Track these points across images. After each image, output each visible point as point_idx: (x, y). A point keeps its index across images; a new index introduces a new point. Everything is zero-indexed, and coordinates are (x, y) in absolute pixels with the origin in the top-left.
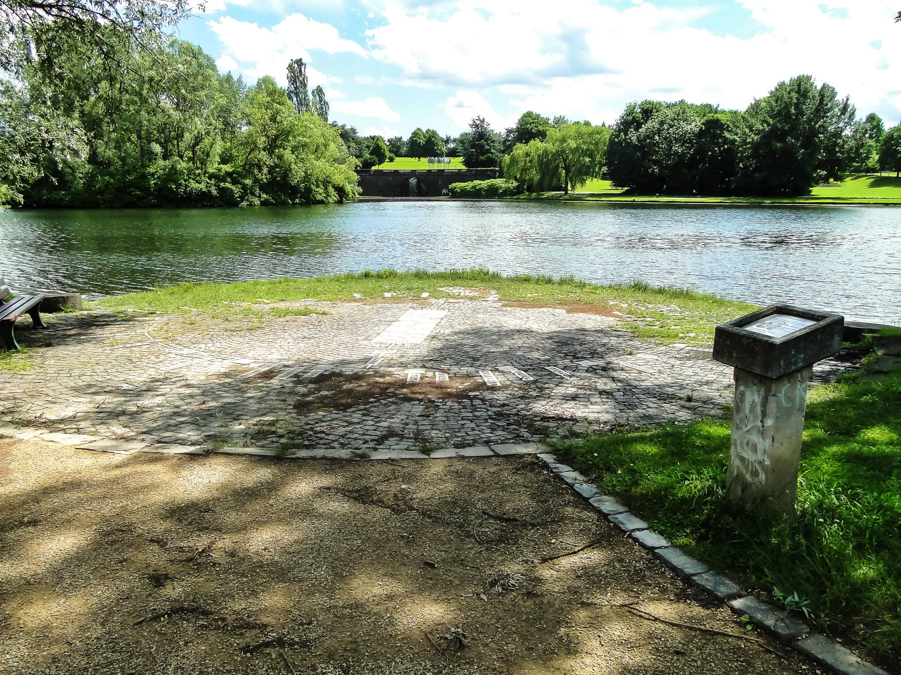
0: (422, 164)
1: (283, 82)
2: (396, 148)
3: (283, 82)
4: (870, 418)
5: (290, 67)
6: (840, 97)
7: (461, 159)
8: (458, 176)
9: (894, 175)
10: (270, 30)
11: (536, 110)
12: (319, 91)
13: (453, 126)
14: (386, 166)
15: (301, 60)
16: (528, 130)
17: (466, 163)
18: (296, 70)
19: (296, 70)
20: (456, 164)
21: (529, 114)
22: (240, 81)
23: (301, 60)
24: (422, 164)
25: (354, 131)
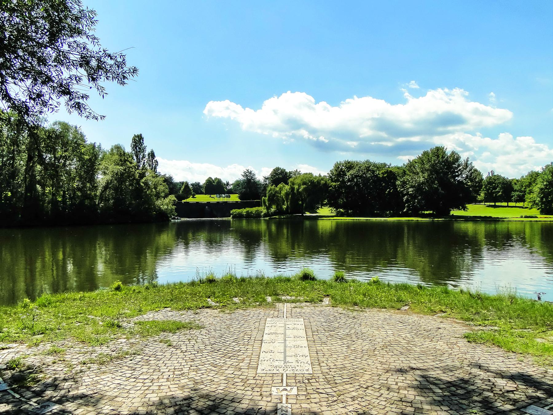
0: (214, 199)
1: (128, 149)
2: (197, 189)
3: (128, 149)
4: (14, 384)
5: (134, 139)
6: (462, 160)
7: (237, 195)
8: (235, 205)
9: (493, 204)
10: (373, 119)
11: (282, 167)
12: (152, 155)
13: (231, 175)
14: (190, 200)
15: (141, 135)
16: (280, 177)
17: (240, 198)
18: (138, 141)
19: (138, 141)
20: (234, 198)
21: (278, 169)
22: (99, 147)
23: (141, 135)
24: (214, 199)
25: (171, 178)
